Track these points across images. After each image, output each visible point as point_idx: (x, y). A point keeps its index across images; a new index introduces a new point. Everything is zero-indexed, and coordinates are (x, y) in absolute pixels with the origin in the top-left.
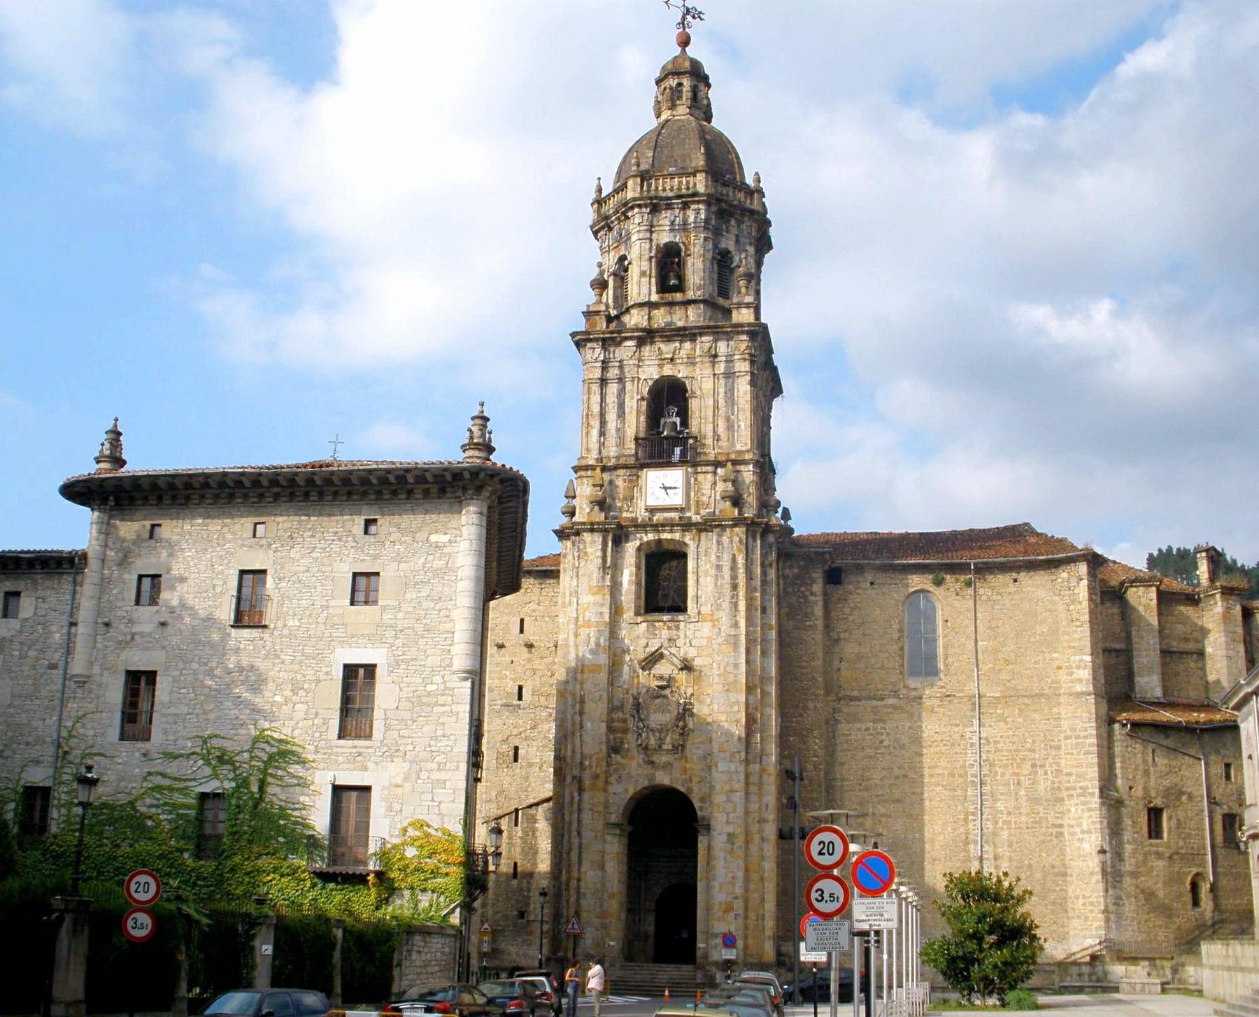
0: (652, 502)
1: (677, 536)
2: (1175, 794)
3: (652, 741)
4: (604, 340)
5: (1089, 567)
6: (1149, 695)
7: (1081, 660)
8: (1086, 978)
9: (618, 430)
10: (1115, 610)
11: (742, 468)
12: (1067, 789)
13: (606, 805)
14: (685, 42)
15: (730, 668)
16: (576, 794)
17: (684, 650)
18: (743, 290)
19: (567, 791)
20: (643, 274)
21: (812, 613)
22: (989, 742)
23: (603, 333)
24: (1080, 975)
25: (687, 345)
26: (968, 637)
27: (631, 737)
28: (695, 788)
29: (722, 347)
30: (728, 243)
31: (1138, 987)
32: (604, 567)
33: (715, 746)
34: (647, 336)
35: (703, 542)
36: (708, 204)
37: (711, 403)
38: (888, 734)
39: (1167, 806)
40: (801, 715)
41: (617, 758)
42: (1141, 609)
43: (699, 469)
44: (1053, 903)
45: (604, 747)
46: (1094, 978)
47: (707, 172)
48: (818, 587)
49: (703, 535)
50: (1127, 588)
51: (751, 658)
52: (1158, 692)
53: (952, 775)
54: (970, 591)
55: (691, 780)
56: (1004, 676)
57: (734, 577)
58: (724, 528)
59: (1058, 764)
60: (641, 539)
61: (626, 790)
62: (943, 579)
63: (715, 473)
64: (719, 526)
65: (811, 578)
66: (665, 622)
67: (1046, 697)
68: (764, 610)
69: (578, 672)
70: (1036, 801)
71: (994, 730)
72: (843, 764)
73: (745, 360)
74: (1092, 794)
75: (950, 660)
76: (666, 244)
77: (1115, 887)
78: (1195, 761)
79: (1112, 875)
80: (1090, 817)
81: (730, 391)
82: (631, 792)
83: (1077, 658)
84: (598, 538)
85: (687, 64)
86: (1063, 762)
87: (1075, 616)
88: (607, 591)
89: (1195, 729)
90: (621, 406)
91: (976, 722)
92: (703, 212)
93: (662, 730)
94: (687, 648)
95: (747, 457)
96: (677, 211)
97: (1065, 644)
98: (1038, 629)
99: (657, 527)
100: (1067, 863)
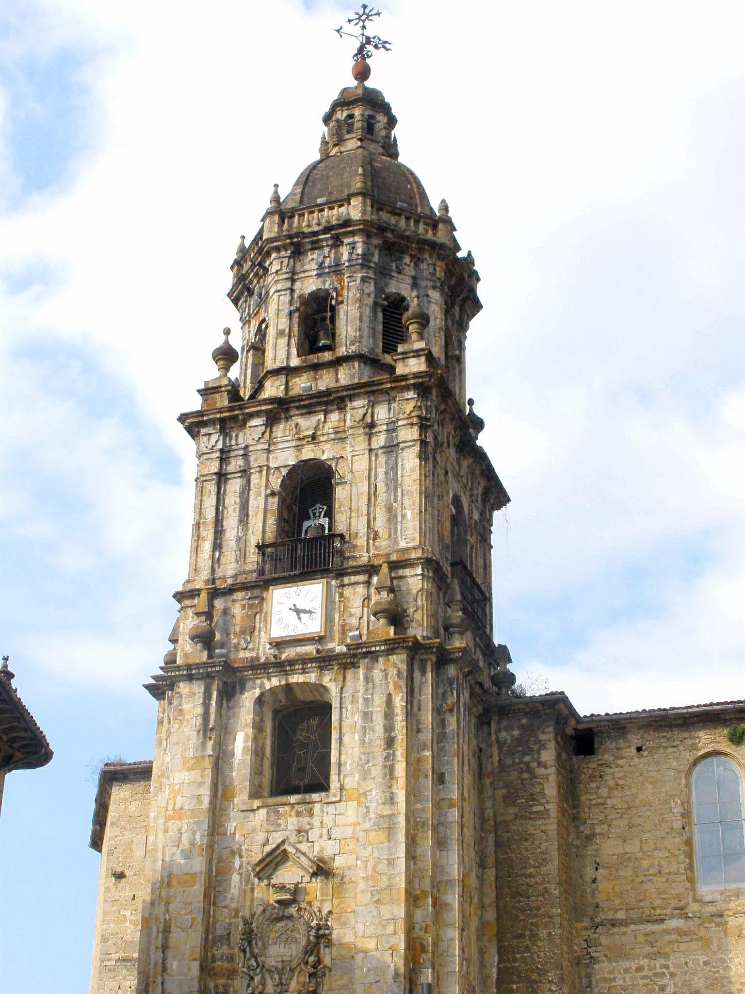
0: (278, 632)
1: (312, 677)
4: (222, 421)
9: (239, 539)
11: (407, 572)
14: (362, 73)
15: (382, 867)
17: (321, 846)
18: (414, 337)
20: (281, 333)
21: (542, 793)
23: (220, 415)
25: (334, 417)
29: (382, 413)
30: (401, 286)
32: (205, 730)
34: (280, 410)
35: (349, 684)
36: (368, 236)
38: (672, 975)
40: (528, 949)
43: (346, 580)
48: (548, 755)
49: (350, 674)
57: (389, 728)
58: (373, 656)
63: (368, 583)
64: (366, 654)
66: (292, 805)
68: (440, 779)
69: (168, 881)
73: (412, 424)
81: (392, 470)
84: (198, 688)
88: (208, 764)
93: (284, 970)
95: (413, 556)
96: (326, 250)
99: (281, 666)
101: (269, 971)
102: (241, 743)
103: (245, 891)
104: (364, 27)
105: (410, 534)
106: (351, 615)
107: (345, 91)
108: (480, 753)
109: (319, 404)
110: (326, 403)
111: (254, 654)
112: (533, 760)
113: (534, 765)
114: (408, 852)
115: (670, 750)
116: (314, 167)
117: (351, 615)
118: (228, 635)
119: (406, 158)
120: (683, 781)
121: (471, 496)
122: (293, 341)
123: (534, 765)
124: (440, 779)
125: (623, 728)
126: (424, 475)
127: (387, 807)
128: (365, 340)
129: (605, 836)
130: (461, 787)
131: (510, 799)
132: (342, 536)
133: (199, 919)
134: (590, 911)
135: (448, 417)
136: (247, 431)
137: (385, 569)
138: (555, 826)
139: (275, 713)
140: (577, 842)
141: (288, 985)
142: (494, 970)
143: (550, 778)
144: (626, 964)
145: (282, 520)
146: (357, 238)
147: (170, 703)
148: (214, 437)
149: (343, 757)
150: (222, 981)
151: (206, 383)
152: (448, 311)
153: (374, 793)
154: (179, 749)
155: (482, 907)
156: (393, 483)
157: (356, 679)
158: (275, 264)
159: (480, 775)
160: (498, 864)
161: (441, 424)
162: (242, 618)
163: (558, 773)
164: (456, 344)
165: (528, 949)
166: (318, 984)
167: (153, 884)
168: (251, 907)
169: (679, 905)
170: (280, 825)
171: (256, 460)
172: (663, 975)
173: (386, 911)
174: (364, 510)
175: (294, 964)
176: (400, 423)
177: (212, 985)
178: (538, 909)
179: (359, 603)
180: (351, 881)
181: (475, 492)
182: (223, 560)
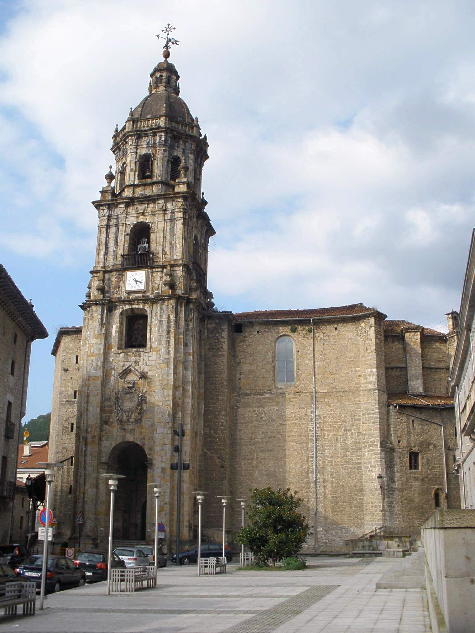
0: (128, 288)
1: (141, 306)
2: (426, 445)
3: (125, 417)
4: (109, 205)
5: (375, 320)
6: (416, 391)
7: (371, 371)
8: (367, 548)
9: (114, 251)
10: (400, 346)
11: (176, 268)
12: (364, 443)
13: (100, 452)
14: (167, 55)
15: (165, 377)
16: (84, 447)
17: (143, 367)
18: (183, 175)
19: (81, 445)
20: (131, 170)
21: (222, 348)
22: (320, 418)
23: (109, 201)
24: (363, 547)
25: (151, 206)
26: (310, 360)
27: (114, 415)
29: (169, 206)
30: (178, 153)
31: (392, 553)
32: (102, 324)
33: (156, 419)
34: (130, 202)
35: (154, 309)
37: (162, 234)
38: (265, 414)
39: (422, 452)
40: (215, 404)
41: (106, 427)
42: (412, 344)
43: (154, 270)
44: (355, 507)
45: (99, 421)
46: (371, 548)
47: (166, 116)
48: (225, 334)
49: (155, 306)
50: (404, 333)
51: (178, 371)
52: (421, 390)
53: (300, 436)
54: (311, 335)
55: (144, 439)
56: (329, 381)
57: (168, 327)
58: (164, 300)
59: (359, 429)
60: (122, 308)
61: (111, 444)
62: (296, 329)
63: (162, 272)
65: (221, 329)
67: (354, 392)
68: (186, 345)
69: (88, 379)
70: (347, 449)
71: (323, 411)
73: (180, 211)
74: (376, 445)
75: (300, 372)
76: (144, 155)
77: (389, 497)
78: (438, 427)
79: (387, 490)
80: (375, 458)
81: (172, 228)
82: (114, 445)
83: (369, 370)
84: (99, 308)
85: (166, 65)
86: (361, 429)
88: (103, 337)
89: (437, 409)
91: (314, 406)
92: (163, 137)
93: (130, 411)
94: (144, 366)
95: (179, 262)
97: (363, 363)
99: (130, 302)
100: (363, 483)
101: (124, 412)
102: (114, 329)
104: (168, 34)
105: (178, 254)
107: (160, 64)
108: (200, 333)
109: (146, 200)
110: (149, 200)
111: (119, 296)
112: (219, 335)
113: (220, 337)
116: (146, 99)
118: (110, 288)
123: (220, 337)
124: (186, 345)
126: (184, 232)
128: (164, 175)
129: (244, 363)
130: (193, 347)
132: (153, 254)
134: (238, 390)
135: (194, 207)
136: (118, 209)
137: (169, 267)
139: (127, 317)
140: (234, 365)
142: (203, 410)
146: (163, 134)
147: (88, 313)
148: (106, 211)
150: (108, 414)
151: (103, 188)
154: (92, 330)
155: (199, 388)
156: (173, 234)
157: (157, 307)
158: (130, 141)
159: (200, 340)
160: (206, 372)
163: (228, 340)
165: (215, 404)
166: (141, 417)
167: (83, 379)
168: (118, 389)
172: (262, 413)
173: (166, 392)
174: (162, 244)
175: (133, 409)
176: (176, 210)
177: (104, 416)
178: (219, 389)
179: (159, 279)
180: (154, 381)
182: (108, 259)
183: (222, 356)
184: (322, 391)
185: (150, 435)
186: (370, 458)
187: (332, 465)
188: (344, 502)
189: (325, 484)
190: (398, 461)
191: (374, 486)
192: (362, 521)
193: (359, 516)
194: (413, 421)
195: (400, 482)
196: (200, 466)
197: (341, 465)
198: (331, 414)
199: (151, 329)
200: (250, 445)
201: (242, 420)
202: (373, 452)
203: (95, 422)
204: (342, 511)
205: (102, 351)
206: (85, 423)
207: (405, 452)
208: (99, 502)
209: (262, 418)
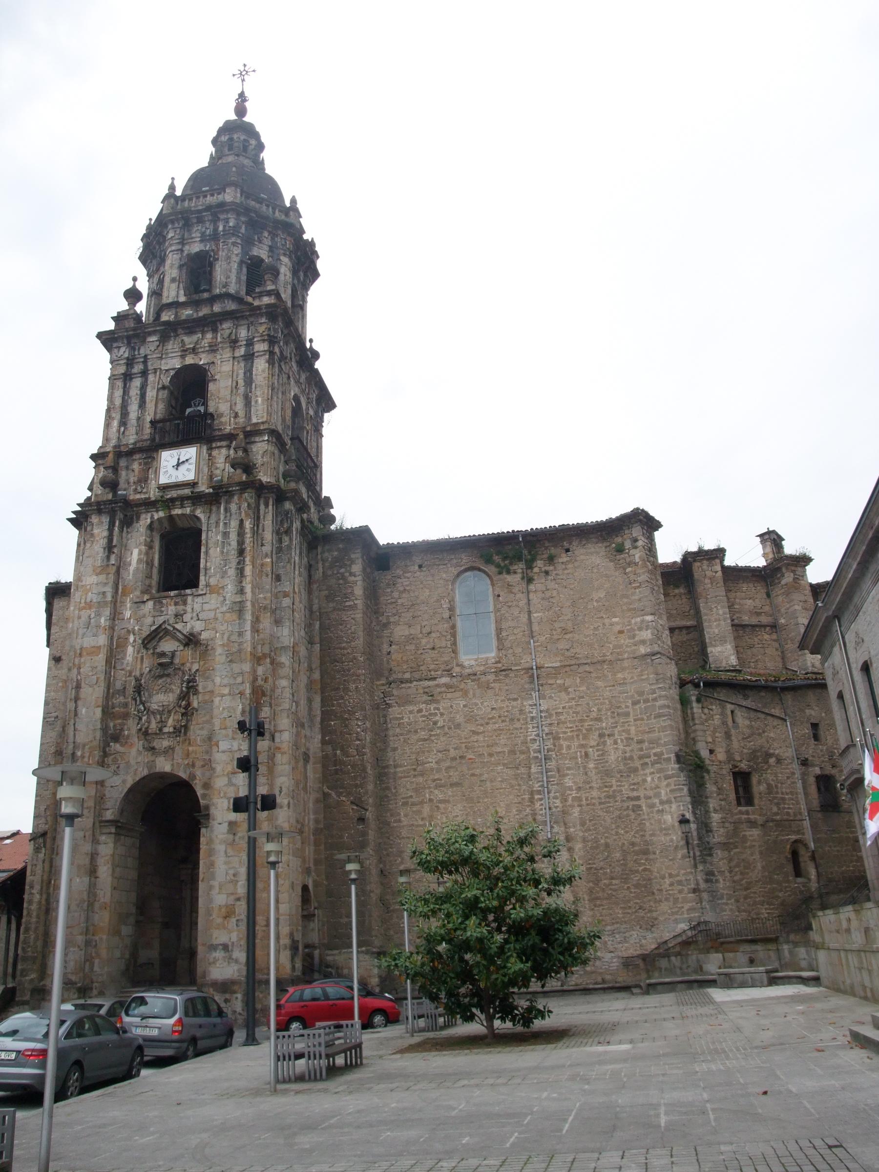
0: (163, 480)
1: (188, 511)
2: (763, 757)
3: (153, 726)
6: (724, 664)
9: (138, 419)
15: (234, 638)
21: (352, 593)
28: (198, 773)
38: (442, 714)
39: (755, 770)
40: (342, 698)
41: (115, 747)
44: (637, 886)
45: (98, 734)
53: (512, 752)
55: (193, 765)
56: (562, 645)
57: (241, 543)
58: (230, 494)
59: (628, 732)
60: (152, 517)
61: (124, 782)
70: (608, 773)
72: (395, 749)
73: (264, 341)
75: (504, 634)
77: (704, 862)
80: (668, 785)
83: (638, 619)
87: (632, 577)
89: (776, 688)
90: (143, 396)
93: (165, 711)
98: (595, 596)
102: (135, 556)
103: (137, 658)
106: (217, 468)
108: (310, 568)
111: (147, 496)
114: (253, 627)
115: (441, 567)
117: (217, 468)
119: (268, 171)
120: (450, 587)
121: (308, 398)
122: (181, 285)
123: (347, 574)
125: (410, 553)
127: (238, 596)
129: (397, 624)
131: (329, 598)
132: (212, 415)
133: (103, 678)
134: (386, 673)
137: (241, 436)
138: (361, 615)
139: (163, 537)
141: (166, 722)
143: (358, 583)
144: (411, 708)
145: (170, 406)
148: (123, 349)
149: (208, 564)
152: (295, 273)
153: (229, 587)
156: (249, 380)
161: (286, 343)
162: (139, 472)
163: (364, 580)
164: (300, 298)
165: (342, 698)
166: (188, 721)
168: (141, 669)
169: (447, 668)
170: (162, 612)
171: (152, 365)
173: (236, 668)
177: (112, 725)
178: (349, 670)
181: (311, 396)
182: (127, 433)
183: (354, 607)
184: (550, 665)
185: (207, 757)
186: (657, 787)
187: (580, 806)
188: (612, 878)
189: (570, 845)
190: (714, 789)
191: (672, 840)
192: (655, 914)
193: (647, 906)
194: (732, 712)
195: (722, 830)
196: (317, 821)
197: (600, 803)
198: (570, 707)
199: (207, 553)
200: (415, 776)
201: (398, 730)
202: (662, 775)
203: (91, 737)
204: (610, 897)
205: (109, 598)
206: (71, 740)
207: (724, 772)
208: (97, 905)
209: (435, 723)
